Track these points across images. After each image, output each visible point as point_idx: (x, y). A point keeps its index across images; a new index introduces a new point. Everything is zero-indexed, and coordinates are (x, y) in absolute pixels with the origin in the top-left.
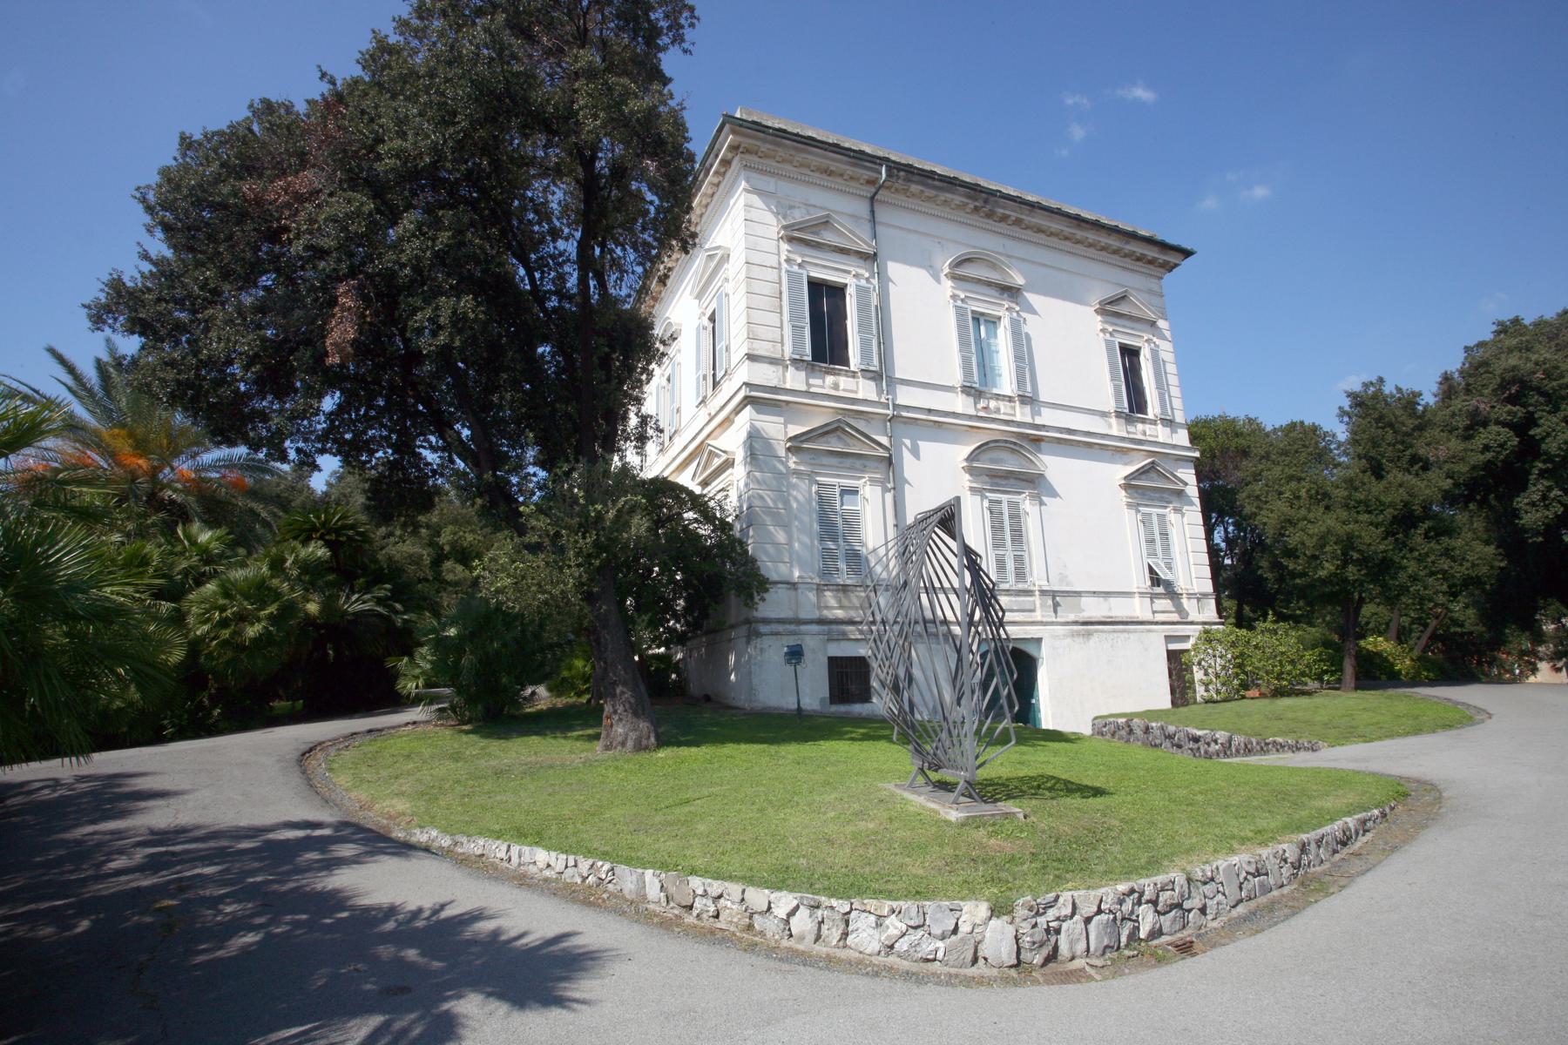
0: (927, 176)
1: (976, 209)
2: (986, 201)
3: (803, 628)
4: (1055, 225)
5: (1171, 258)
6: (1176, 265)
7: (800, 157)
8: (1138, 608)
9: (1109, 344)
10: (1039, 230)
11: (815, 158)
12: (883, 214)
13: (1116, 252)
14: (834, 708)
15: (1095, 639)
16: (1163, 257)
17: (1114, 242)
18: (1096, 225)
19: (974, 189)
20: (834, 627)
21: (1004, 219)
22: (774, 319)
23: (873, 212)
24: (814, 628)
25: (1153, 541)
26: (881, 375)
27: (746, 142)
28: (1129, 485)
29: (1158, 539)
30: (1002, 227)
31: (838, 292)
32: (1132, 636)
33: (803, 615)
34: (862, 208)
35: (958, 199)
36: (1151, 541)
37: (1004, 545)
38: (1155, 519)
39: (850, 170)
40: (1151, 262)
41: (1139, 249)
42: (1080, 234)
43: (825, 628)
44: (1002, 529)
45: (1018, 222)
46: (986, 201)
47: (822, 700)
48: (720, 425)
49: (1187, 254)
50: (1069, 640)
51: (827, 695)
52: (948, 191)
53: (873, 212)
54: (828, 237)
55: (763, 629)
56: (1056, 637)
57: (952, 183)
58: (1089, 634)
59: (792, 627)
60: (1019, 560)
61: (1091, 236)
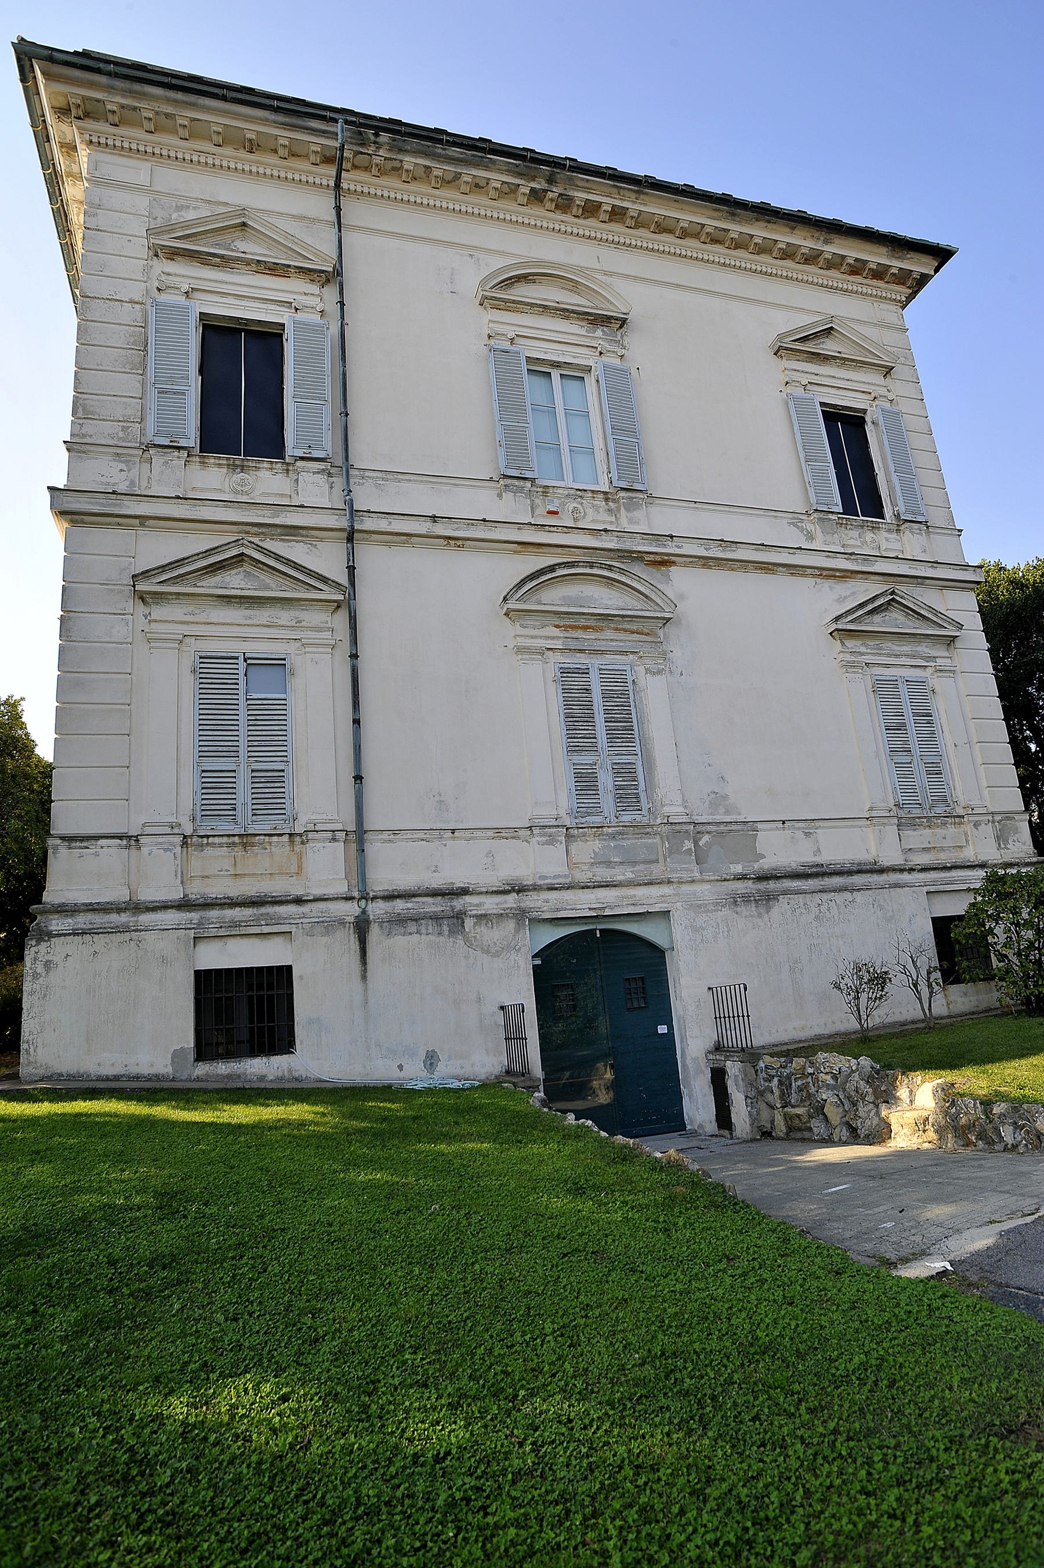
0: (432, 139)
1: (536, 197)
2: (551, 180)
3: (146, 918)
4: (688, 215)
5: (917, 265)
6: (923, 280)
7: (470, 173)
8: (883, 846)
9: (795, 406)
10: (662, 228)
11: (216, 116)
12: (355, 211)
13: (811, 259)
14: (203, 1069)
15: (781, 907)
16: (896, 264)
17: (804, 241)
18: (764, 212)
19: (526, 160)
20: (214, 914)
21: (591, 210)
22: (130, 384)
23: (338, 209)
24: (172, 917)
25: (901, 727)
26: (342, 466)
27: (77, 93)
28: (843, 633)
29: (907, 726)
30: (591, 225)
31: (268, 340)
32: (859, 896)
33: (147, 895)
34: (322, 206)
35: (497, 178)
36: (896, 728)
37: (593, 748)
38: (903, 689)
39: (285, 136)
40: (879, 274)
41: (852, 251)
42: (736, 229)
43: (195, 916)
44: (589, 719)
45: (617, 214)
46: (551, 180)
47: (176, 1055)
48: (219, 596)
49: (942, 255)
50: (726, 912)
51: (190, 1042)
52: (477, 165)
53: (338, 209)
54: (829, 347)
55: (56, 924)
56: (696, 907)
57: (481, 149)
58: (769, 898)
59: (124, 918)
60: (624, 772)
61: (759, 231)
